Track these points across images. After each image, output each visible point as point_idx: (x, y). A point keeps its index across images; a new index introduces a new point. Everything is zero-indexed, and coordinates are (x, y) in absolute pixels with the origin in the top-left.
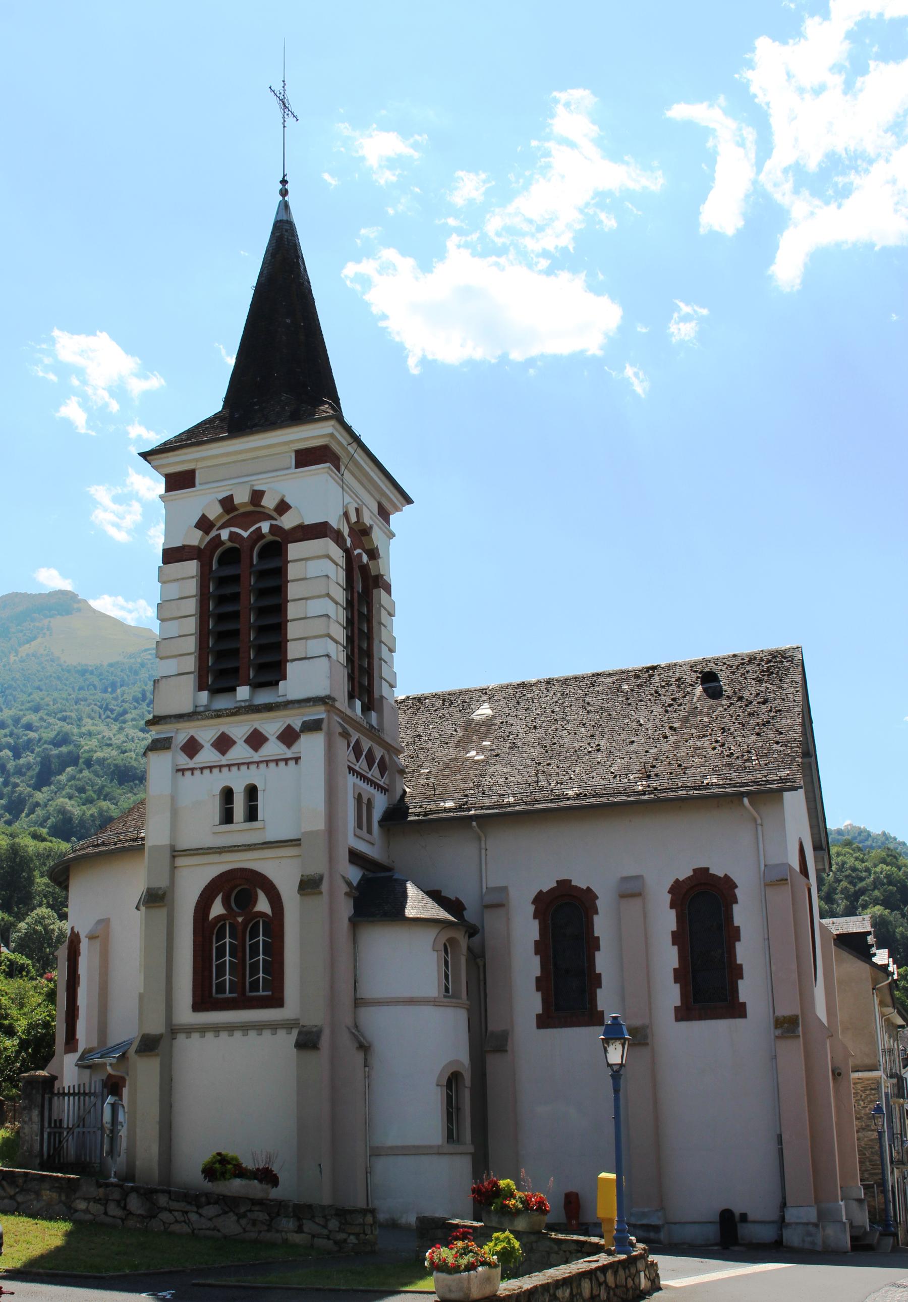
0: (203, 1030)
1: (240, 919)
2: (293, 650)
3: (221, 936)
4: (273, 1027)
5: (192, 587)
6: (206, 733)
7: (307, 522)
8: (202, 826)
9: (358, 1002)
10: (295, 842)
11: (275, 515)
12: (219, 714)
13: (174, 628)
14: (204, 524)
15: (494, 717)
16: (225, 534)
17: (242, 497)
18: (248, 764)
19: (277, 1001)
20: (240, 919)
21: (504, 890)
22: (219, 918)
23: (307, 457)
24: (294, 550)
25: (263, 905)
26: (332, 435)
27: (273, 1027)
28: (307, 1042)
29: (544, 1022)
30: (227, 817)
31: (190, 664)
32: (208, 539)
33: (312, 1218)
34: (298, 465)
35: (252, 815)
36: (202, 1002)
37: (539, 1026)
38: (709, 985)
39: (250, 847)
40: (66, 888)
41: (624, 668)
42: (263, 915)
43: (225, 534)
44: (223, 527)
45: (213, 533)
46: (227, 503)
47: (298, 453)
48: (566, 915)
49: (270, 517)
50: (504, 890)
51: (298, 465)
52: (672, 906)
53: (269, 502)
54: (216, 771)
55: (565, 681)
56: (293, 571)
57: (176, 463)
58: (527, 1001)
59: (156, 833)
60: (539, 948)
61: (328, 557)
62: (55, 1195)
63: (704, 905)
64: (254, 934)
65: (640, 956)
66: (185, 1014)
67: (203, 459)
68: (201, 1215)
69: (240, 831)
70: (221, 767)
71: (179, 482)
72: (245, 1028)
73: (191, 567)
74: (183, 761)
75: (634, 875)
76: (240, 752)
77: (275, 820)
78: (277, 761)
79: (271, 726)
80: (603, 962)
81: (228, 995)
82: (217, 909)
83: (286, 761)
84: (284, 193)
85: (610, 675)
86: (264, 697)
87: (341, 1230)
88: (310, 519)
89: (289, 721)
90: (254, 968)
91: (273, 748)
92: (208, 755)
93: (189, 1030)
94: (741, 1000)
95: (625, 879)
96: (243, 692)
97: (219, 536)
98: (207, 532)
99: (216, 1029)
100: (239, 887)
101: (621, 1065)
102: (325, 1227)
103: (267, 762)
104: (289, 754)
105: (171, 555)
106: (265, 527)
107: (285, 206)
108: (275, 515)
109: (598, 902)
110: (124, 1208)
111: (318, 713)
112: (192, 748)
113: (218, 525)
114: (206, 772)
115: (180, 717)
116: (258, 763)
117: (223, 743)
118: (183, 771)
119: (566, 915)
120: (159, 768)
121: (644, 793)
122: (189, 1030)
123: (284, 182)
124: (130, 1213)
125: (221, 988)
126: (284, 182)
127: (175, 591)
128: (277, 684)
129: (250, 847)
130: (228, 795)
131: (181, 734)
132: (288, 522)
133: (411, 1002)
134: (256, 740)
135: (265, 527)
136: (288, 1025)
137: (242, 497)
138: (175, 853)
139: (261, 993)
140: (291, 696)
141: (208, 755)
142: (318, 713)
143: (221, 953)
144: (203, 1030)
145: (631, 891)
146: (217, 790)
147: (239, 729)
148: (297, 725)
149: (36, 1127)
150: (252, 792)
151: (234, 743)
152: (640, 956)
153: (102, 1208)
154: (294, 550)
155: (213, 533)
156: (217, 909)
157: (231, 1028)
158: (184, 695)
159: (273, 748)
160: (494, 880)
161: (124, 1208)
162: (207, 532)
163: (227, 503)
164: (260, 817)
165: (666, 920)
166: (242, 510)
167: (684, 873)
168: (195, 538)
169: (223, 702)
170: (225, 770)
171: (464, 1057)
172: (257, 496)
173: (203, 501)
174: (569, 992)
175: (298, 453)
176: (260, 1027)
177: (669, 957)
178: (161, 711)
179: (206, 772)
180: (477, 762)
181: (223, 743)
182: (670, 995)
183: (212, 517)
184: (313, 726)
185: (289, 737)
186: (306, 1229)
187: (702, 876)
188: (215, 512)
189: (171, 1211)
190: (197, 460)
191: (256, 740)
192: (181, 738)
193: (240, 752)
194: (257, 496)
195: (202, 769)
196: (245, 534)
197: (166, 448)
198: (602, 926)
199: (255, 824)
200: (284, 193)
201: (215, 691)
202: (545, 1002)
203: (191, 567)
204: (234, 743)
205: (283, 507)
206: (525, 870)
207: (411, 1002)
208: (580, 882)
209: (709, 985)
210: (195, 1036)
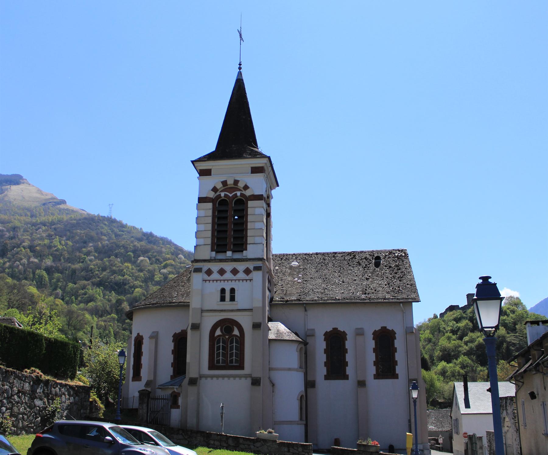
0: (212, 377)
1: (227, 337)
2: (249, 240)
3: (218, 342)
4: (240, 377)
5: (210, 213)
6: (215, 267)
7: (255, 194)
8: (213, 302)
9: (270, 369)
10: (251, 310)
11: (242, 189)
12: (221, 261)
13: (202, 227)
14: (215, 190)
15: (300, 266)
16: (223, 194)
17: (230, 182)
18: (232, 280)
19: (241, 367)
20: (227, 337)
21: (314, 330)
22: (219, 336)
23: (256, 170)
24: (250, 203)
25: (236, 332)
26: (266, 163)
27: (240, 377)
28: (256, 382)
29: (327, 378)
30: (223, 299)
31: (209, 241)
32: (216, 195)
33: (293, 448)
34: (252, 172)
35: (232, 299)
36: (212, 366)
37: (325, 379)
38: (386, 367)
39: (232, 311)
40: (131, 319)
41: (344, 251)
42: (236, 336)
43: (223, 194)
44: (221, 191)
45: (218, 193)
46: (224, 183)
47: (252, 168)
48: (336, 340)
49: (240, 190)
50: (314, 330)
51: (252, 172)
52: (373, 339)
53: (241, 185)
54: (219, 282)
55: (323, 254)
56: (250, 211)
57: (203, 166)
58: (321, 370)
59: (195, 303)
60: (326, 351)
61: (263, 207)
62: (202, 439)
63: (384, 340)
64: (232, 342)
65: (361, 355)
66: (205, 369)
67: (216, 166)
68: (254, 446)
69: (227, 304)
70: (221, 280)
71: (203, 173)
72: (223, 377)
73: (210, 205)
74: (206, 277)
75: (359, 329)
76: (228, 275)
77: (242, 301)
78: (243, 280)
79: (241, 267)
80: (349, 357)
81: (221, 364)
82: (218, 332)
83: (246, 280)
84: (240, 68)
85: (339, 253)
86: (237, 256)
87: (303, 451)
88: (256, 193)
89: (248, 266)
90: (231, 355)
91: (241, 275)
92: (216, 276)
93: (206, 377)
94: (397, 373)
95: (357, 329)
96: (229, 254)
97: (220, 195)
98: (216, 193)
99: (218, 377)
100: (227, 325)
101: (416, 398)
102: (297, 450)
103: (239, 280)
104: (247, 278)
105: (201, 200)
106: (239, 193)
107: (240, 74)
108: (242, 189)
109: (347, 336)
110: (227, 443)
111: (259, 264)
112: (209, 272)
113: (220, 190)
114: (215, 282)
115: (205, 261)
116: (235, 280)
117: (222, 272)
118: (206, 281)
119: (336, 340)
120: (197, 278)
121: (366, 300)
122: (206, 377)
123: (240, 64)
124: (229, 445)
125: (218, 361)
126: (240, 64)
127: (203, 213)
128: (242, 251)
129: (232, 311)
130: (223, 291)
131: (206, 266)
132: (248, 193)
133: (289, 369)
134: (235, 272)
135: (239, 193)
136: (246, 376)
137: (230, 182)
138: (202, 311)
139: (234, 364)
140: (250, 256)
141: (216, 276)
142: (259, 264)
143: (218, 348)
144: (212, 377)
145: (360, 333)
146: (219, 289)
147: (228, 267)
148: (251, 268)
149: (145, 411)
150: (233, 291)
151: (226, 272)
152: (361, 355)
153: (219, 443)
154: (250, 203)
155: (218, 193)
156: (218, 332)
157: (223, 377)
158: (207, 253)
159: (241, 275)
160: (310, 326)
161: (227, 443)
162: (216, 193)
163: (224, 183)
164: (236, 300)
165: (372, 344)
166: (229, 186)
167: (378, 328)
168: (212, 195)
169: (221, 256)
170: (222, 282)
171: (303, 389)
172: (236, 182)
173: (214, 181)
174: (336, 368)
175: (252, 168)
176: (235, 377)
177: (371, 357)
178: (198, 258)
179: (215, 282)
180: (299, 282)
181: (222, 272)
182: (372, 370)
183: (218, 188)
184: (257, 268)
185: (247, 271)
186: (291, 451)
187: (384, 329)
188: (219, 186)
189: (244, 445)
190: (213, 166)
191: (235, 272)
192: (205, 269)
193: (228, 275)
194: (236, 182)
195: (213, 281)
196: (231, 195)
197: (200, 160)
198: (349, 344)
199: (234, 303)
200: (240, 68)
201: (217, 252)
202: (328, 371)
203: (210, 205)
204: (226, 272)
205: (246, 187)
206: (322, 323)
207: (289, 369)
208: (341, 329)
209: (386, 367)
210: (209, 379)
